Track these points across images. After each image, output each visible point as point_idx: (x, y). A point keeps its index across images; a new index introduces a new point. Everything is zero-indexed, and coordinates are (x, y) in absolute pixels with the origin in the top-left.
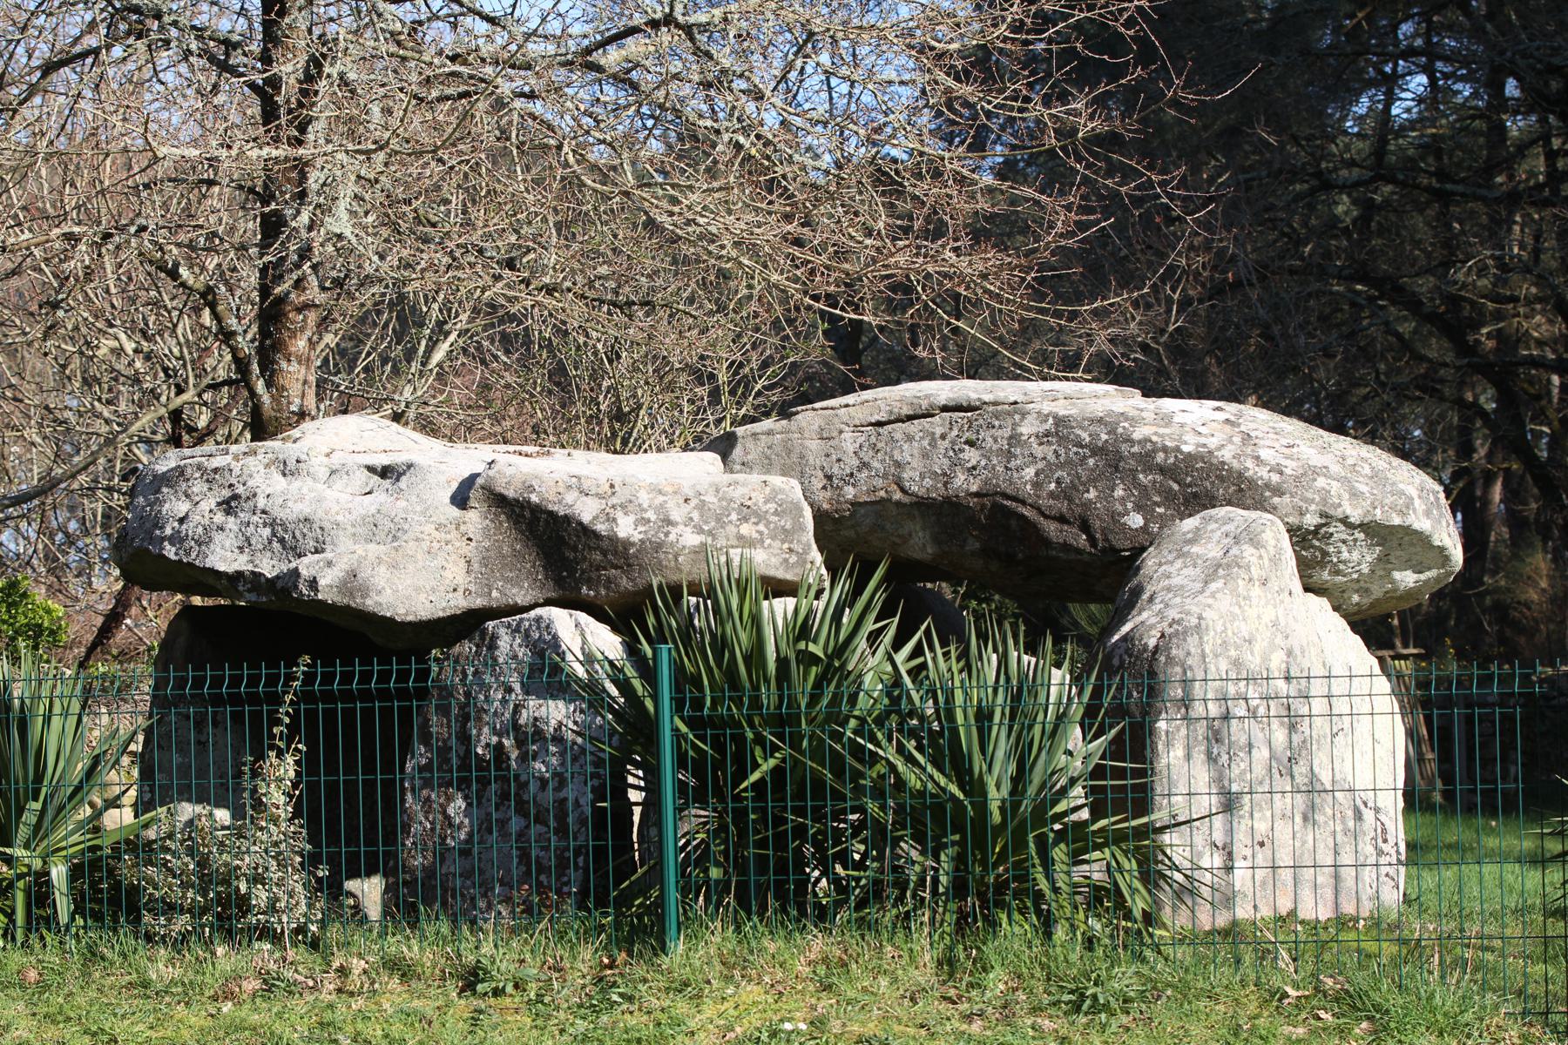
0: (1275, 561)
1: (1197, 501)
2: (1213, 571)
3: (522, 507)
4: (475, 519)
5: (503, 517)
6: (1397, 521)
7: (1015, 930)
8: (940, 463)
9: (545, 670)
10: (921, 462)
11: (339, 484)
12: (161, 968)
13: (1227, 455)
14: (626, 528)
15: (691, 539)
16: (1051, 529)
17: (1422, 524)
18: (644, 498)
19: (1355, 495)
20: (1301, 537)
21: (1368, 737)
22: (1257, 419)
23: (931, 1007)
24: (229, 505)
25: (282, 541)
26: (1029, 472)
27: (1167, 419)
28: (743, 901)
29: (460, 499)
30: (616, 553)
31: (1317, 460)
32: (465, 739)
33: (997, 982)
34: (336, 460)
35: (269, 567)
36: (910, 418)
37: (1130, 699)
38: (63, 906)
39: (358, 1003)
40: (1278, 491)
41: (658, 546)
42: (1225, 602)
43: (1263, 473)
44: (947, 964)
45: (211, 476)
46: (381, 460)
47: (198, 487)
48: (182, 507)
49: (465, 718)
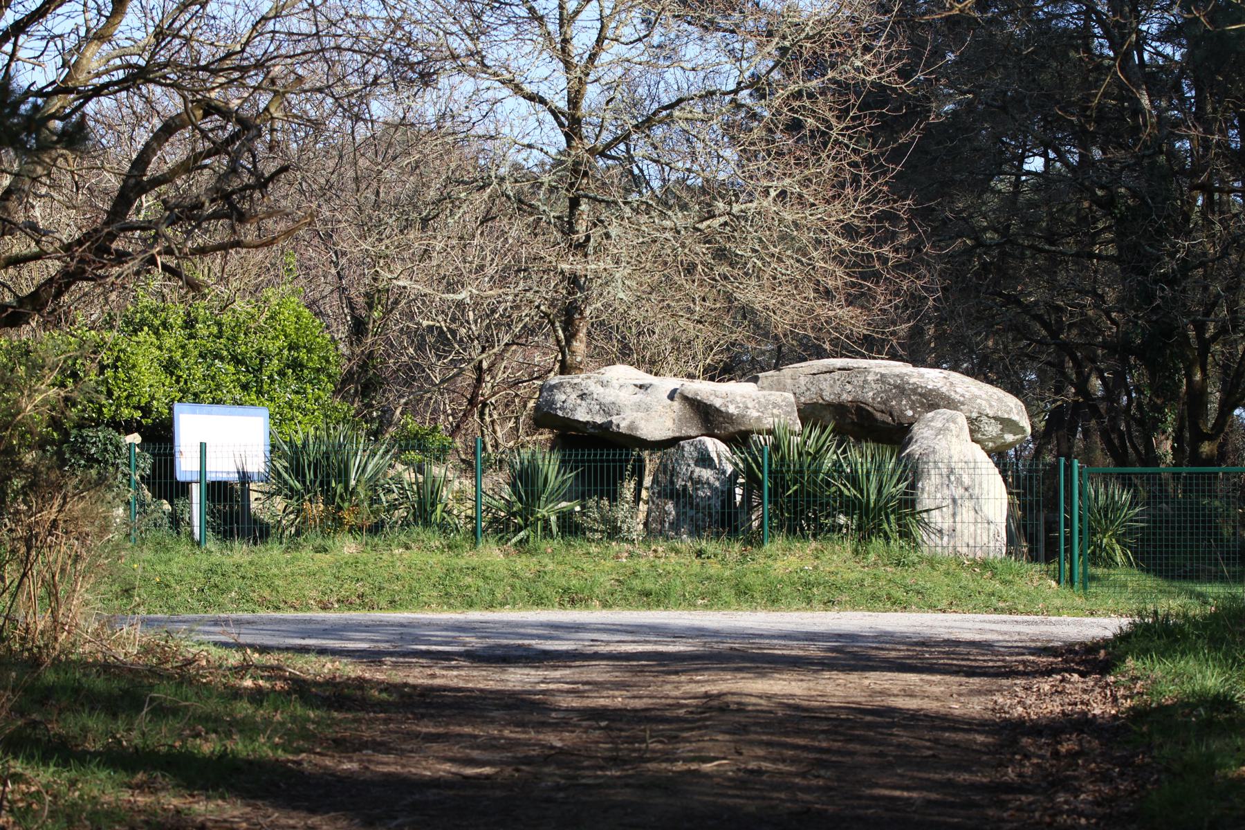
0: (961, 429)
1: (933, 406)
2: (940, 431)
4: (676, 404)
6: (1006, 416)
7: (877, 543)
8: (837, 390)
9: (704, 460)
10: (830, 390)
11: (624, 390)
12: (594, 549)
13: (944, 390)
14: (732, 409)
15: (755, 414)
16: (878, 415)
17: (1015, 418)
18: (738, 399)
19: (991, 406)
20: (971, 421)
21: (995, 499)
22: (956, 377)
23: (851, 563)
24: (582, 396)
26: (871, 394)
27: (922, 376)
28: (789, 531)
29: (671, 397)
31: (977, 392)
32: (672, 483)
33: (872, 557)
34: (622, 381)
35: (599, 420)
37: (912, 473)
38: (555, 529)
39: (663, 560)
40: (963, 404)
42: (944, 443)
43: (957, 397)
44: (856, 552)
45: (574, 386)
46: (639, 383)
47: (569, 390)
48: (563, 397)
49: (672, 475)
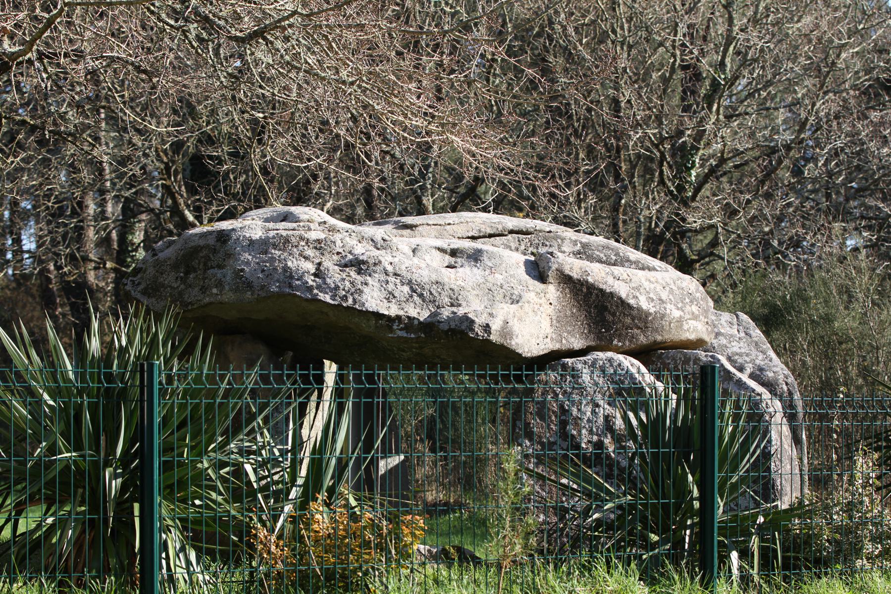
3: (582, 285)
5: (567, 290)
25: (421, 296)
30: (640, 319)
35: (719, 312)
36: (491, 236)
41: (663, 316)
49: (563, 424)
